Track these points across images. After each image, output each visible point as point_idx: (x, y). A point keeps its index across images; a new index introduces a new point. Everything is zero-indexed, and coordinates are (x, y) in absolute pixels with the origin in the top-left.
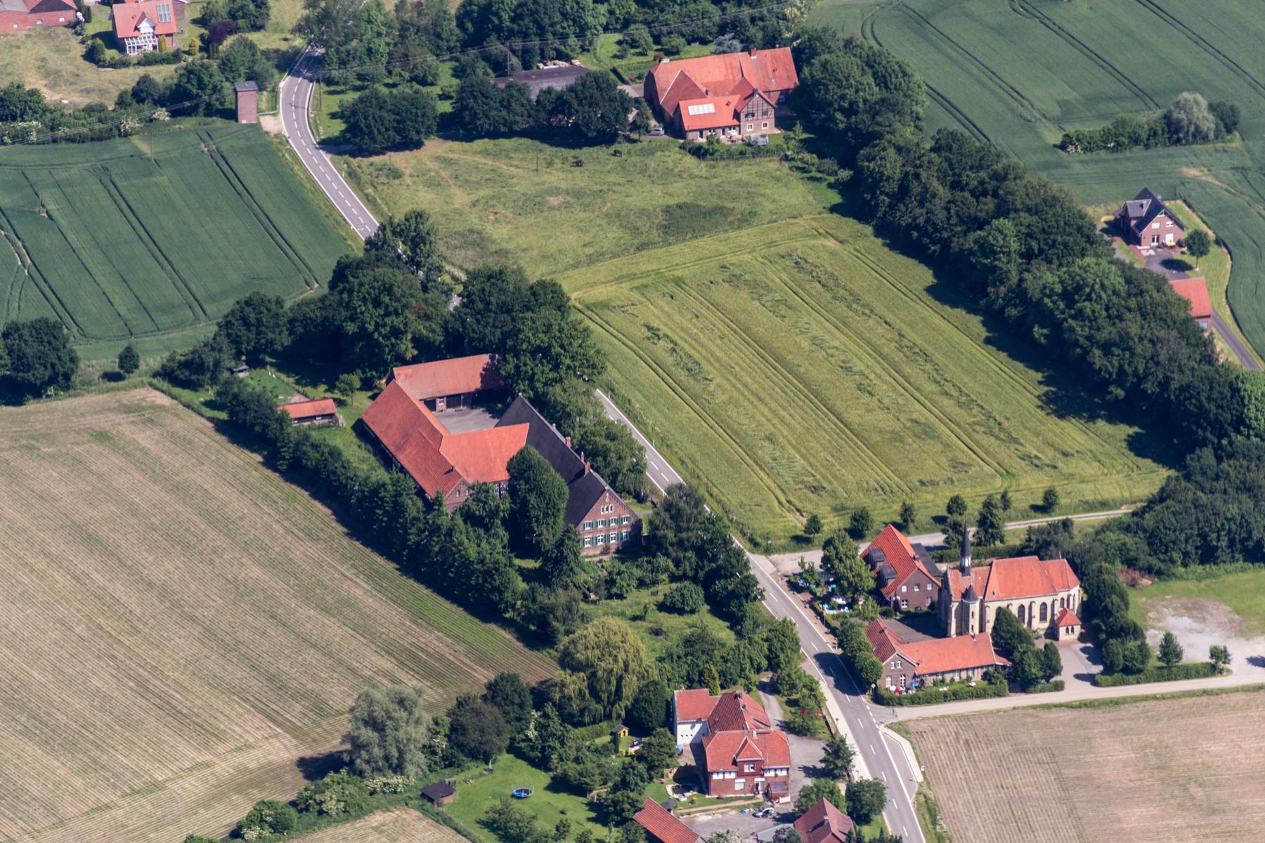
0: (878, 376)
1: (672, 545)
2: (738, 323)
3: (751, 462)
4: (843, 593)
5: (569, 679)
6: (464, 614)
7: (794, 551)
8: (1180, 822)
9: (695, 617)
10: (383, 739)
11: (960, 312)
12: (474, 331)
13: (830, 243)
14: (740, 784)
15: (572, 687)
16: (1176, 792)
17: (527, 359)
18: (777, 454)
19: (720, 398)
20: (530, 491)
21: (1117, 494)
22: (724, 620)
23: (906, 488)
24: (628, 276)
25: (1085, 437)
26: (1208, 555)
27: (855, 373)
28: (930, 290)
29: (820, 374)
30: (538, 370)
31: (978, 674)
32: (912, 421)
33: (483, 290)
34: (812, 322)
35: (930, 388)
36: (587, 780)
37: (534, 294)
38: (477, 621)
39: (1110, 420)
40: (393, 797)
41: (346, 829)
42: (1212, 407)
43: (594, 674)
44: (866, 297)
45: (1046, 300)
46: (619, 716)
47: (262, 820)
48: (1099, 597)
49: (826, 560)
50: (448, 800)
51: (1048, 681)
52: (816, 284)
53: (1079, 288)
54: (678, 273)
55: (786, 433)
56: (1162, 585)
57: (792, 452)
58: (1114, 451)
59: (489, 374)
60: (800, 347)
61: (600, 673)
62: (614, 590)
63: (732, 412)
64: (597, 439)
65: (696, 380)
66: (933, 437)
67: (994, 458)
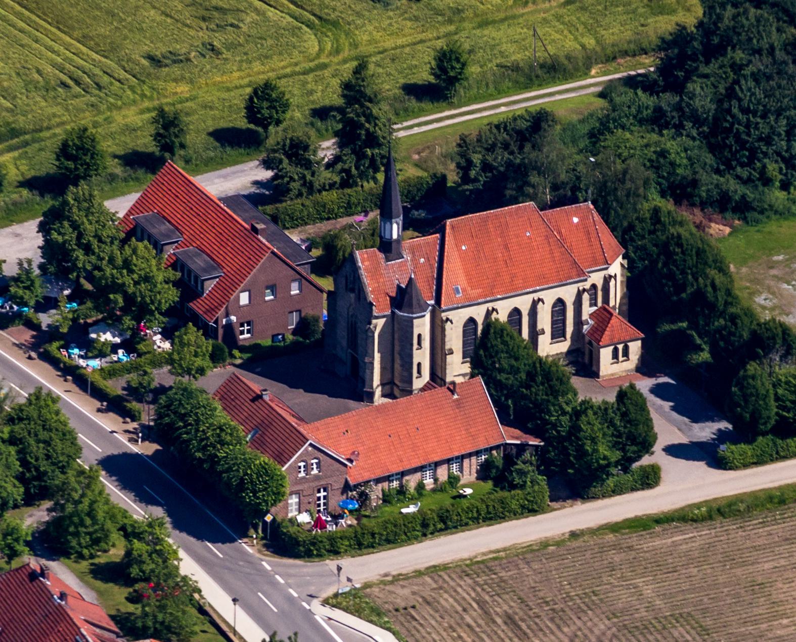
4: (111, 322)
21: (570, 44)
23: (123, 75)
31: (469, 472)
48: (671, 276)
51: (626, 470)
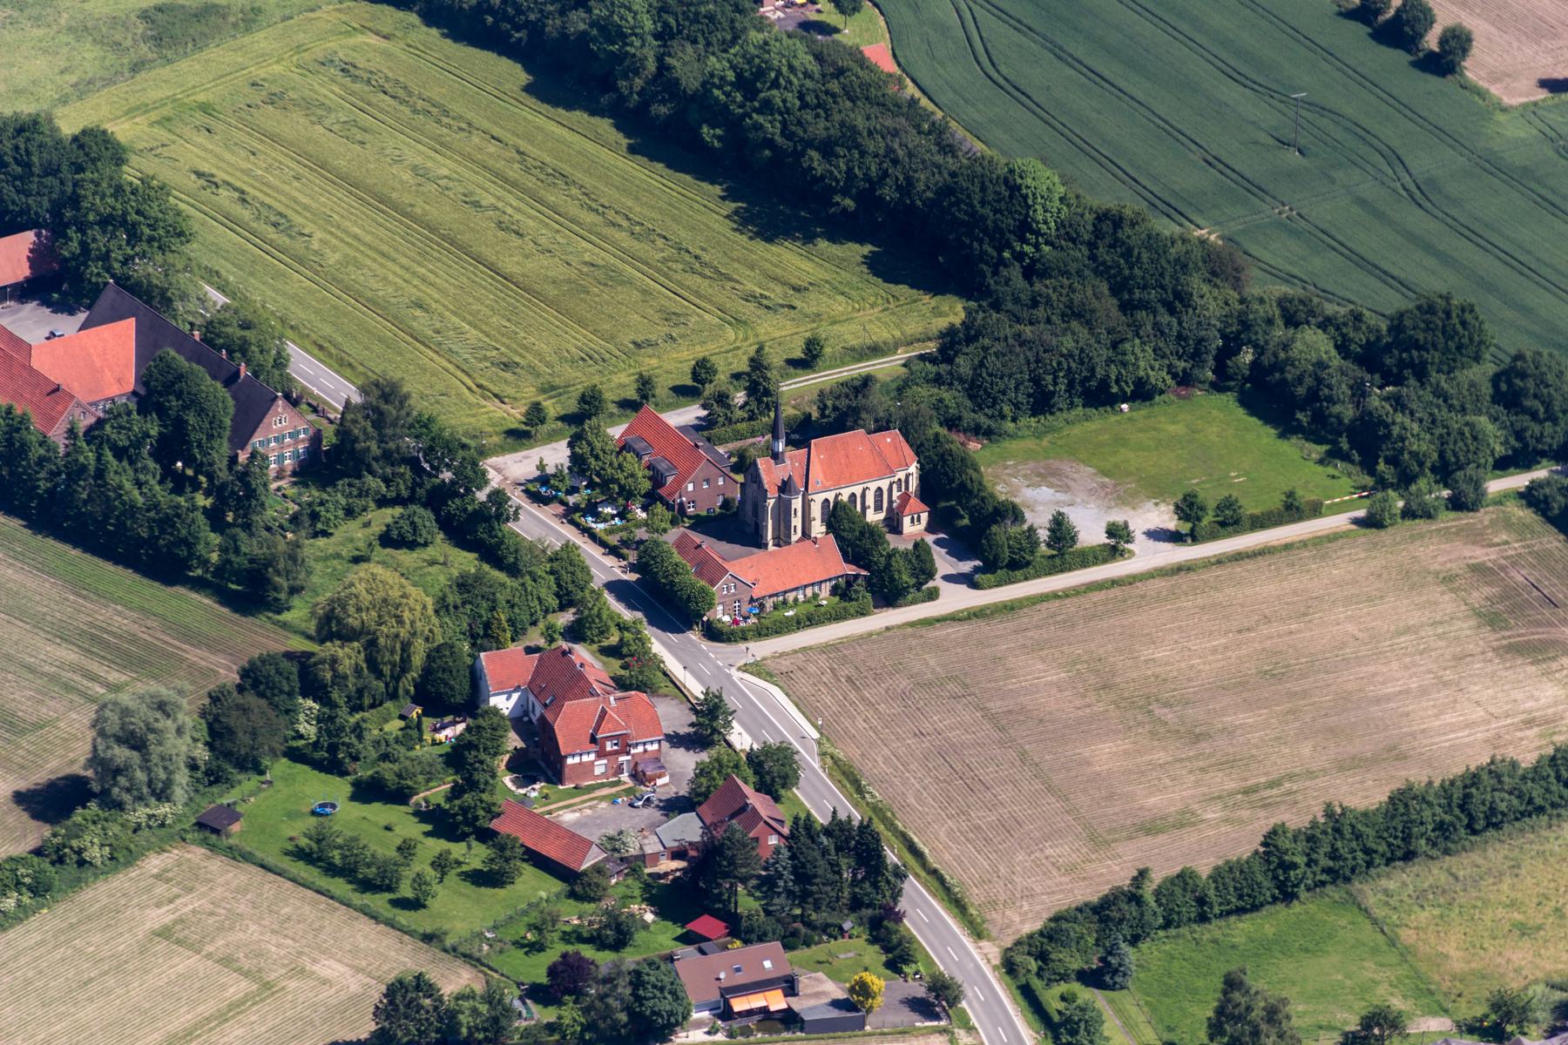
0: (518, 209)
1: (376, 459)
2: (309, 157)
3: (408, 338)
4: (611, 501)
5: (340, 653)
6: (137, 577)
7: (516, 451)
8: (1161, 756)
9: (430, 549)
10: (146, 758)
11: (579, 116)
12: (13, 202)
13: (373, 40)
14: (600, 767)
15: (347, 662)
16: (1140, 717)
17: (95, 232)
18: (438, 325)
19: (332, 258)
20: (185, 408)
21: (885, 335)
22: (470, 551)
24: (138, 108)
25: (810, 264)
26: (1042, 404)
27: (487, 208)
28: (528, 89)
29: (446, 214)
30: (113, 245)
31: (826, 587)
32: (586, 263)
33: (17, 148)
34: (401, 146)
35: (590, 218)
36: (409, 783)
37: (81, 147)
38: (157, 584)
39: (833, 239)
40: (163, 834)
41: (120, 881)
42: (986, 211)
43: (372, 644)
44: (456, 108)
45: (716, 92)
46: (407, 692)
47: (18, 884)
49: (576, 459)
50: (236, 828)
52: (382, 96)
53: (760, 74)
54: (202, 97)
55: (437, 296)
56: (995, 448)
57: (455, 319)
58: (855, 279)
59: (38, 256)
60: (402, 182)
61: (382, 641)
62: (320, 526)
63: (354, 274)
64: (229, 330)
65: (290, 236)
66: (623, 283)
67: (710, 301)
